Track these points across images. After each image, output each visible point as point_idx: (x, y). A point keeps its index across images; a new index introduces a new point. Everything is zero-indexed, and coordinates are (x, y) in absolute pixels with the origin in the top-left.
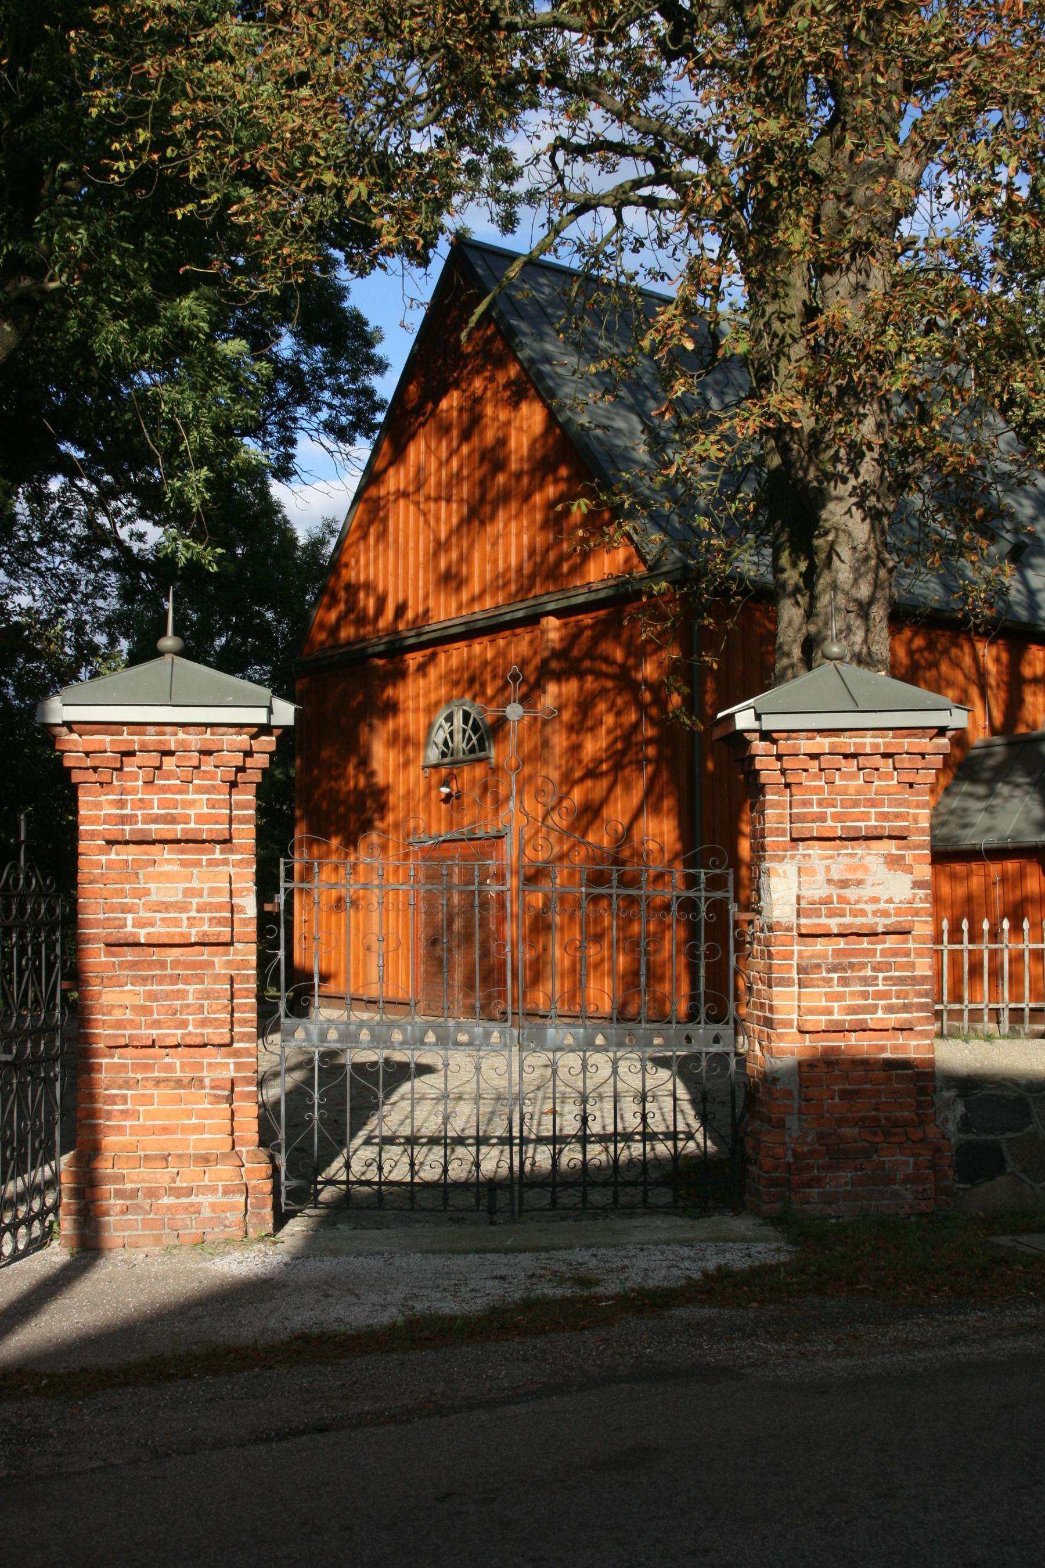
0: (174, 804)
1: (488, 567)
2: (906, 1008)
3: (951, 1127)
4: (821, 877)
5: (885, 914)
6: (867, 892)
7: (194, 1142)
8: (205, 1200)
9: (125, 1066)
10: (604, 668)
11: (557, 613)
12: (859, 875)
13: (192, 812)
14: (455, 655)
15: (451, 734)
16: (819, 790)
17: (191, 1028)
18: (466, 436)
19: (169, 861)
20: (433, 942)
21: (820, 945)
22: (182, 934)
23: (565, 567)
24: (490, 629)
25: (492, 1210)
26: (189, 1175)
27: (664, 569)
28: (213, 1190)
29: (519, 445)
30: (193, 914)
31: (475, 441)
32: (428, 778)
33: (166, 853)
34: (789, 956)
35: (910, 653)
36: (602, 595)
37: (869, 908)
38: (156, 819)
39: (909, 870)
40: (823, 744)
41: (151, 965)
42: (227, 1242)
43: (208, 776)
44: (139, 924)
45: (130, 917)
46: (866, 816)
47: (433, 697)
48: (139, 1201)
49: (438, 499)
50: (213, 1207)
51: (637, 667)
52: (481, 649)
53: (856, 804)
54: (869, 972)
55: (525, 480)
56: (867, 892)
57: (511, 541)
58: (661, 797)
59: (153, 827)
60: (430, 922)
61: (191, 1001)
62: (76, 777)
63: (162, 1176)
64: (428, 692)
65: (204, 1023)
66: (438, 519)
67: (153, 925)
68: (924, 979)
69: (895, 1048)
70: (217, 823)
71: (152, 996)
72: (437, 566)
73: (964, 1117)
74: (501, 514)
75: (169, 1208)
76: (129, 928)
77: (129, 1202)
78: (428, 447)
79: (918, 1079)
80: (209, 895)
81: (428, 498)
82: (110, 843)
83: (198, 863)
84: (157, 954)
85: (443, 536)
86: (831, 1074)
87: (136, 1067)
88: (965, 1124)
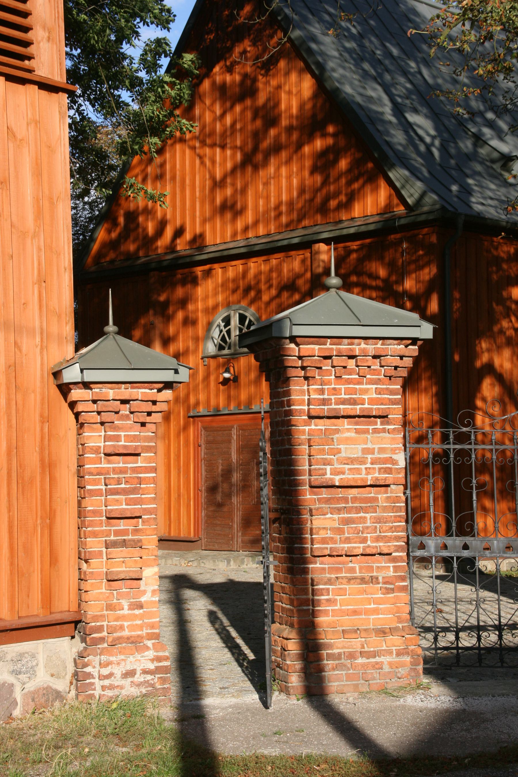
1: (261, 202)
7: (373, 621)
8: (385, 659)
9: (324, 569)
10: (368, 281)
11: (327, 241)
13: (366, 397)
14: (234, 269)
15: (229, 332)
17: (369, 543)
18: (241, 98)
19: (348, 430)
20: (212, 489)
22: (362, 479)
23: (333, 203)
24: (267, 251)
26: (375, 643)
27: (426, 209)
28: (390, 653)
29: (289, 108)
30: (369, 465)
32: (208, 366)
33: (345, 424)
36: (372, 227)
38: (344, 402)
41: (339, 500)
42: (401, 688)
43: (376, 372)
44: (335, 472)
45: (328, 468)
47: (211, 302)
48: (343, 661)
50: (390, 664)
51: (401, 281)
52: (254, 266)
55: (295, 136)
57: (284, 181)
59: (342, 407)
61: (368, 524)
62: (292, 372)
63: (356, 644)
65: (378, 539)
66: (213, 162)
67: (343, 473)
70: (382, 404)
71: (347, 522)
72: (213, 200)
74: (272, 160)
75: (363, 665)
76: (328, 476)
77: (337, 662)
80: (379, 453)
82: (311, 417)
83: (367, 431)
84: (340, 493)
85: (218, 176)
87: (331, 570)
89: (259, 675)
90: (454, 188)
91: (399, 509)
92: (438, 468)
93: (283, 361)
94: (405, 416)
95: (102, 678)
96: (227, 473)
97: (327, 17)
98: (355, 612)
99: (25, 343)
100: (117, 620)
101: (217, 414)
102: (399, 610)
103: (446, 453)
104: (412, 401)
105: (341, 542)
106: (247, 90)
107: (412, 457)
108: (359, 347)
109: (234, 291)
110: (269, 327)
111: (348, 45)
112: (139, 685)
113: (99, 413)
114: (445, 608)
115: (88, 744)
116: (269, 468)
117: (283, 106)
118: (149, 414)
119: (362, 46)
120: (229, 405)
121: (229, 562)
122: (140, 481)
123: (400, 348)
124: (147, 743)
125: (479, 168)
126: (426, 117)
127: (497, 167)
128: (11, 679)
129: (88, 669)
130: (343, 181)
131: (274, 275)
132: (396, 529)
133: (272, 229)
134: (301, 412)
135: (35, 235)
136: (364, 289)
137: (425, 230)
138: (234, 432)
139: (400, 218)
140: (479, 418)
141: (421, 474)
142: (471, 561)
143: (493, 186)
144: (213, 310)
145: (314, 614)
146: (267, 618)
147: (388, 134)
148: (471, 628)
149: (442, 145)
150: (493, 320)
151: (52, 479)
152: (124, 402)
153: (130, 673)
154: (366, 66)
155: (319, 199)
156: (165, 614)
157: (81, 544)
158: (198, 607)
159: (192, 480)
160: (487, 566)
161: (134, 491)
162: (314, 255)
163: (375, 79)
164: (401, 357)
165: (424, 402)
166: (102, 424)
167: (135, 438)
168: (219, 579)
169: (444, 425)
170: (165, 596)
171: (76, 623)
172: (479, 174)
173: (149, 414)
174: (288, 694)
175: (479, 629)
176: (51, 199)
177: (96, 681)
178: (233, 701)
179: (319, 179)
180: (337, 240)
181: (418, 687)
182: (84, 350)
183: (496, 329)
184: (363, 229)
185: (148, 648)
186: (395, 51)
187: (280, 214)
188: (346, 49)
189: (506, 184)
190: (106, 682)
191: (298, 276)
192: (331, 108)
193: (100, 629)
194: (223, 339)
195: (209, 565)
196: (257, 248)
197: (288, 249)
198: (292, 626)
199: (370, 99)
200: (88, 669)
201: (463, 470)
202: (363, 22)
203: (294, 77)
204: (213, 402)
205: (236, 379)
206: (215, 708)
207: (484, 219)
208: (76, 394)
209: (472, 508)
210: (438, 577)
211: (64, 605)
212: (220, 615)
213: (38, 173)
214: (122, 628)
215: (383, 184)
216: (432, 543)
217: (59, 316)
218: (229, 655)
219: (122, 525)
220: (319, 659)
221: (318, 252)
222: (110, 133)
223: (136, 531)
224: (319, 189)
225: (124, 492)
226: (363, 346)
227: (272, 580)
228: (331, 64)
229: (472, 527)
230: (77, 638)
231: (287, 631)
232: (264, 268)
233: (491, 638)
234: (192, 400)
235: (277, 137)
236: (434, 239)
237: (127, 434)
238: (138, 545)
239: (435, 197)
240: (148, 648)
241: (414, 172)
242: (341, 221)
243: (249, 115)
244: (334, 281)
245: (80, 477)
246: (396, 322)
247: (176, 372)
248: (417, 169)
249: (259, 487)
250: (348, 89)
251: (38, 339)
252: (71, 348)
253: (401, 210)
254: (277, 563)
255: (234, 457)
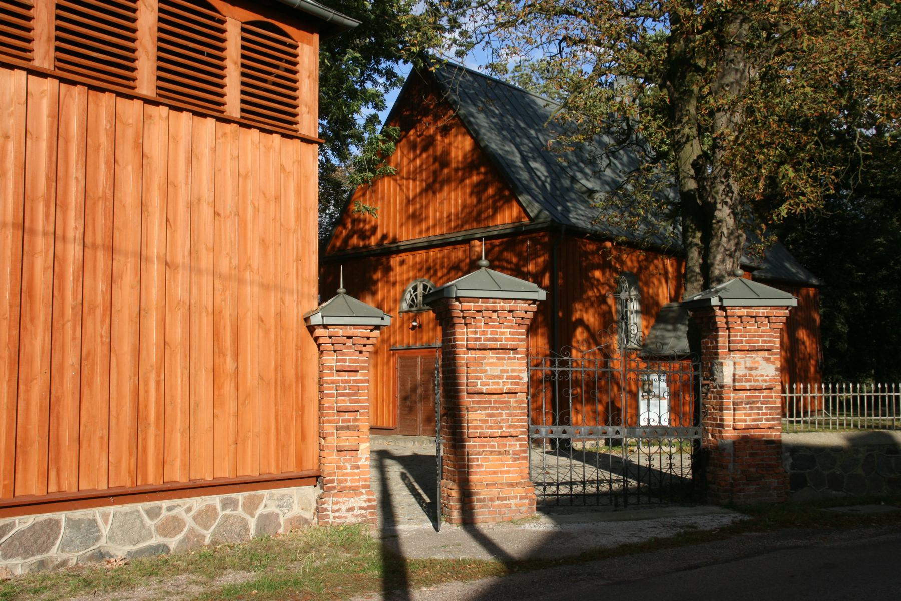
0: (496, 333)
1: (438, 214)
2: (773, 419)
3: (788, 468)
4: (743, 366)
5: (766, 381)
6: (759, 372)
8: (512, 502)
11: (480, 239)
12: (756, 365)
13: (503, 336)
14: (421, 256)
15: (416, 296)
16: (740, 330)
18: (425, 149)
19: (492, 357)
20: (405, 398)
21: (741, 394)
24: (443, 244)
25: (616, 505)
26: (506, 492)
27: (541, 221)
28: (516, 498)
29: (456, 157)
31: (431, 151)
33: (490, 354)
34: (729, 398)
35: (639, 262)
36: (508, 231)
37: (760, 378)
39: (773, 363)
40: (744, 311)
41: (485, 402)
42: (522, 519)
44: (483, 384)
46: (758, 341)
47: (405, 277)
49: (408, 179)
50: (516, 505)
51: (526, 265)
53: (754, 336)
54: (760, 405)
55: (460, 174)
56: (759, 372)
57: (452, 201)
58: (537, 327)
60: (403, 388)
62: (456, 320)
63: (494, 492)
64: (402, 274)
65: (509, 427)
66: (408, 189)
68: (777, 408)
69: (768, 436)
71: (490, 416)
72: (407, 211)
73: (792, 464)
74: (446, 189)
75: (499, 506)
76: (479, 386)
78: (402, 153)
79: (776, 445)
81: (403, 178)
82: (468, 349)
83: (503, 358)
84: (486, 398)
85: (411, 197)
86: (747, 444)
87: (480, 446)
88: (793, 467)
89: (433, 512)
90: (559, 208)
91: (523, 408)
92: (548, 384)
93: (450, 313)
94: (528, 350)
95: (334, 511)
96: (414, 389)
97: (481, 105)
98: (494, 473)
99: (288, 299)
100: (343, 475)
101: (409, 348)
102: (522, 471)
103: (553, 373)
104: (532, 342)
105: (487, 428)
106: (430, 142)
107: (532, 377)
108: (499, 305)
109: (420, 270)
110: (442, 291)
111: (493, 120)
112: (357, 516)
113: (333, 344)
114: (550, 471)
115: (325, 551)
116: (442, 381)
117: (453, 155)
118: (365, 345)
119: (502, 121)
120: (416, 342)
121: (414, 443)
122: (359, 388)
123: (525, 305)
124: (363, 551)
125: (573, 196)
126: (541, 164)
127: (585, 196)
128: (277, 510)
129: (325, 506)
130: (490, 202)
131: (446, 260)
132: (521, 420)
133: (445, 230)
134: (462, 345)
135: (295, 231)
136: (502, 269)
137: (541, 234)
138: (419, 360)
139: (526, 226)
140: (574, 352)
141: (537, 387)
142: (567, 441)
143: (583, 208)
144: (405, 283)
145: (468, 473)
146: (440, 479)
147: (519, 174)
148: (566, 483)
149: (551, 181)
150: (583, 291)
151: (303, 386)
152: (349, 337)
153: (351, 509)
154: (504, 133)
155: (474, 214)
156: (372, 475)
157: (321, 428)
158: (395, 471)
159: (391, 390)
160: (578, 446)
161: (355, 394)
162: (471, 247)
163: (510, 141)
164: (526, 312)
165: (540, 343)
166: (335, 351)
167: (355, 361)
168: (408, 453)
169: (552, 355)
170: (373, 463)
171: (318, 477)
172: (574, 200)
173: (365, 345)
174: (451, 523)
175: (571, 483)
176: (306, 209)
177: (330, 513)
178: (416, 527)
179: (475, 201)
180: (487, 238)
181: (533, 518)
182: (324, 304)
183: (584, 297)
184: (502, 232)
185: (362, 494)
186: (522, 125)
187: (450, 221)
188: (493, 123)
189: (589, 207)
190: (337, 514)
191: (461, 261)
192: (482, 157)
193: (332, 481)
194: (413, 300)
195: (402, 444)
196: (435, 243)
197: (455, 243)
198: (454, 481)
199: (507, 152)
200: (325, 506)
201: (564, 384)
202: (503, 106)
203: (460, 138)
204: (406, 341)
205: (420, 326)
206: (405, 531)
207: (577, 227)
208: (319, 332)
209: (568, 407)
210: (547, 453)
211: (310, 466)
212: (408, 475)
213: (298, 193)
214: (346, 481)
215: (515, 204)
216: (543, 429)
217: (309, 283)
218: (414, 499)
219: (347, 416)
220: (471, 501)
221: (474, 246)
222: (344, 172)
223: (356, 420)
224: (475, 206)
225: (348, 395)
226: (502, 304)
227: (442, 454)
228: (483, 131)
229: (568, 419)
230: (318, 487)
231: (451, 484)
232: (439, 255)
233: (578, 489)
234: (392, 340)
235: (449, 173)
236: (546, 239)
237: (351, 358)
238: (357, 428)
239: (547, 213)
240: (362, 494)
241: (534, 197)
242: (488, 227)
243: (431, 160)
244: (484, 262)
245: (321, 385)
246: (523, 289)
247: (383, 318)
248: (536, 196)
249: (434, 395)
250: (493, 146)
251: (295, 297)
252: (316, 303)
253: (525, 220)
254: (445, 441)
255: (419, 377)
